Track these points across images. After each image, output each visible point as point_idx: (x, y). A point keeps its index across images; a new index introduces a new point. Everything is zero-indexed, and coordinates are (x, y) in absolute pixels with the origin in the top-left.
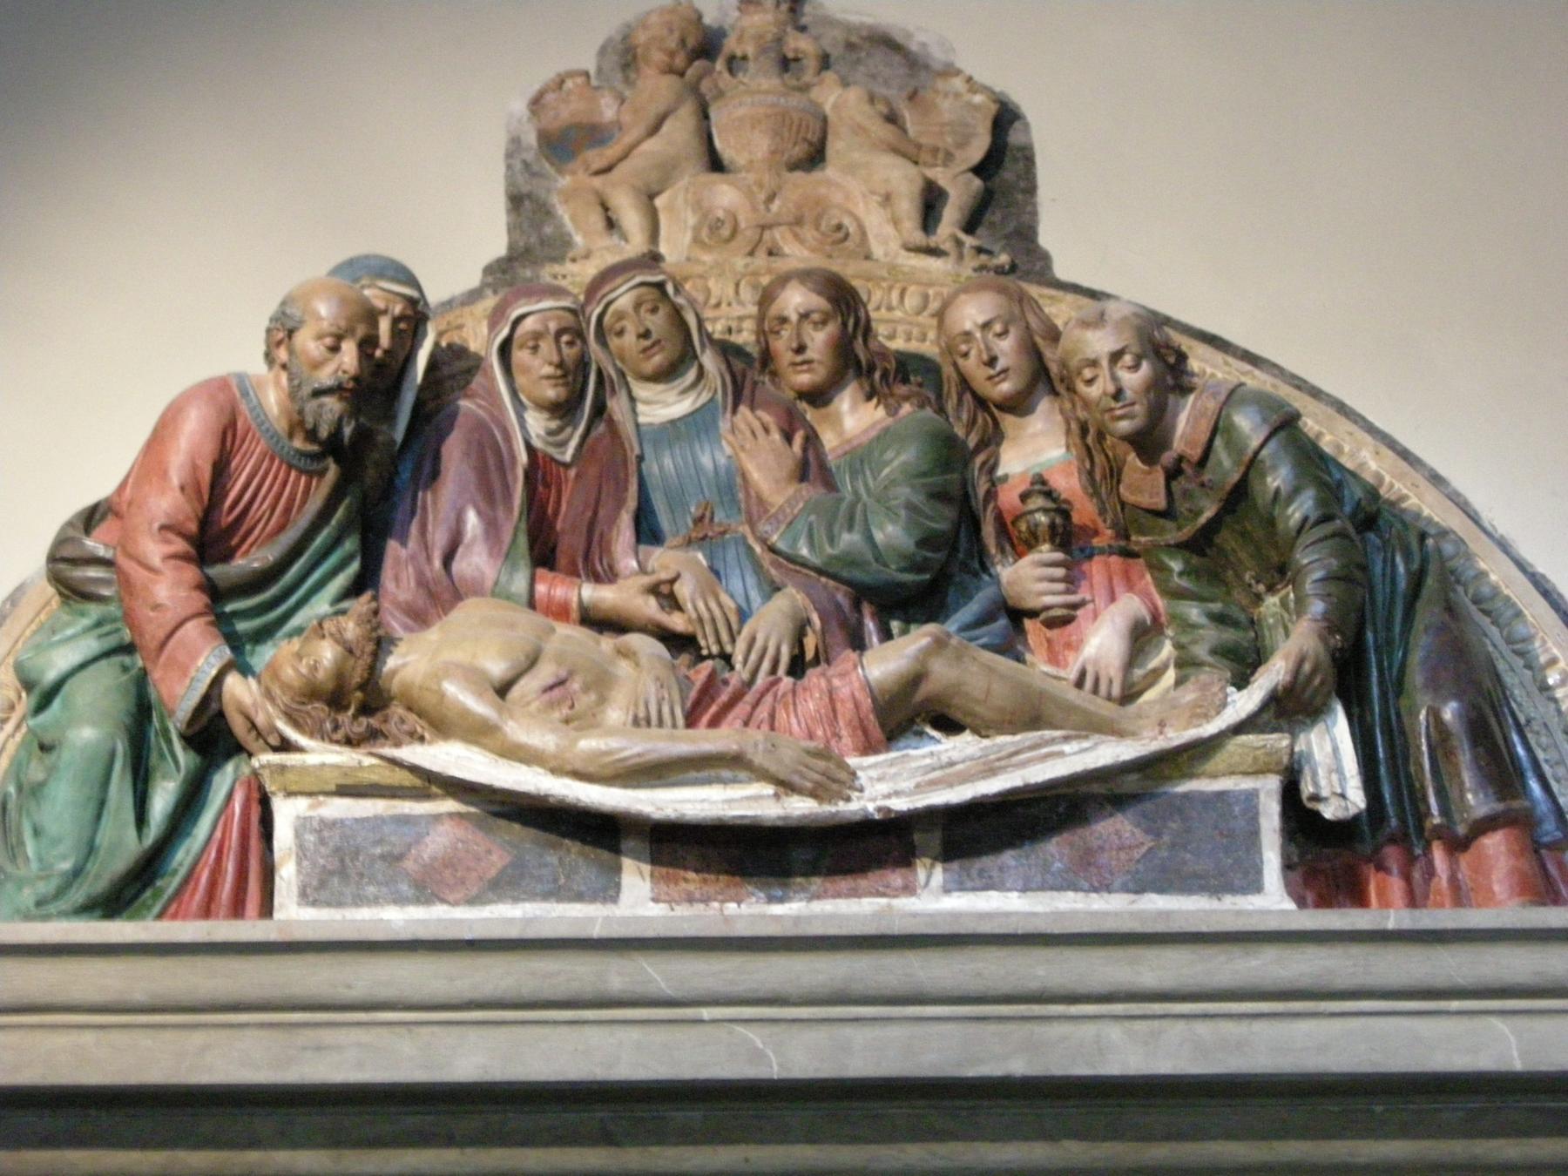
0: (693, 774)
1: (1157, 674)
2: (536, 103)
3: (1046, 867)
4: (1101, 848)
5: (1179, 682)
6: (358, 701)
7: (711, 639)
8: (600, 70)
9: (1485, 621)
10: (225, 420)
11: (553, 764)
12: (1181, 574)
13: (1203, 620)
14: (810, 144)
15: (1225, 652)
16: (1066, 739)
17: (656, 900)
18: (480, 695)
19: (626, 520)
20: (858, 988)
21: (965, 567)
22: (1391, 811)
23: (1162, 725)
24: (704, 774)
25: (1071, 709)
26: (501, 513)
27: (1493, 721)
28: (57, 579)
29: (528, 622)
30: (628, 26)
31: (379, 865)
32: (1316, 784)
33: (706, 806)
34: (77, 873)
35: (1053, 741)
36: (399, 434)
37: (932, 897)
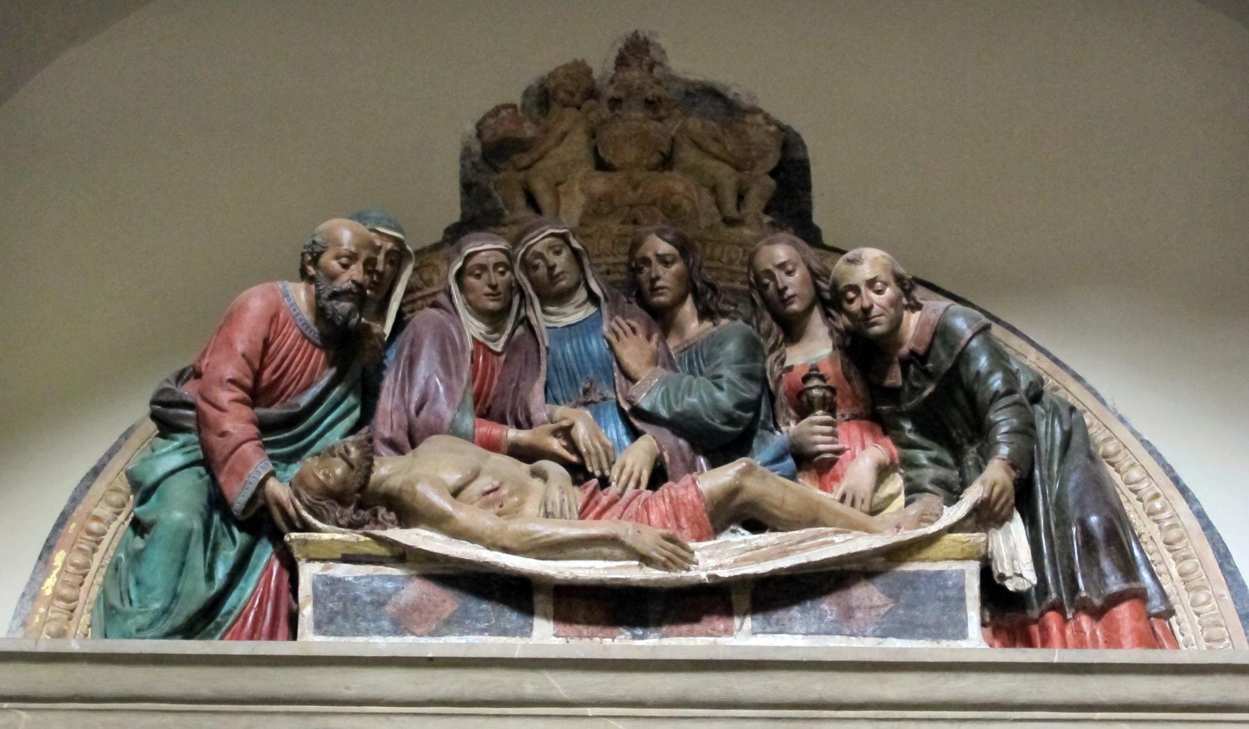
0: (584, 551)
1: (892, 497)
2: (480, 126)
3: (821, 618)
4: (859, 607)
5: (907, 503)
6: (363, 501)
7: (596, 466)
8: (523, 106)
9: (1110, 469)
10: (273, 311)
11: (489, 541)
12: (910, 431)
13: (925, 462)
14: (662, 154)
15: (942, 484)
16: (836, 533)
17: (556, 636)
18: (441, 495)
19: (539, 387)
20: (694, 697)
21: (765, 427)
22: (1052, 588)
23: (898, 527)
24: (592, 550)
25: (838, 514)
26: (454, 381)
27: (1120, 531)
28: (154, 416)
29: (473, 453)
30: (543, 79)
31: (369, 608)
32: (1002, 567)
33: (592, 571)
34: (166, 611)
35: (826, 534)
36: (387, 330)
37: (745, 636)
